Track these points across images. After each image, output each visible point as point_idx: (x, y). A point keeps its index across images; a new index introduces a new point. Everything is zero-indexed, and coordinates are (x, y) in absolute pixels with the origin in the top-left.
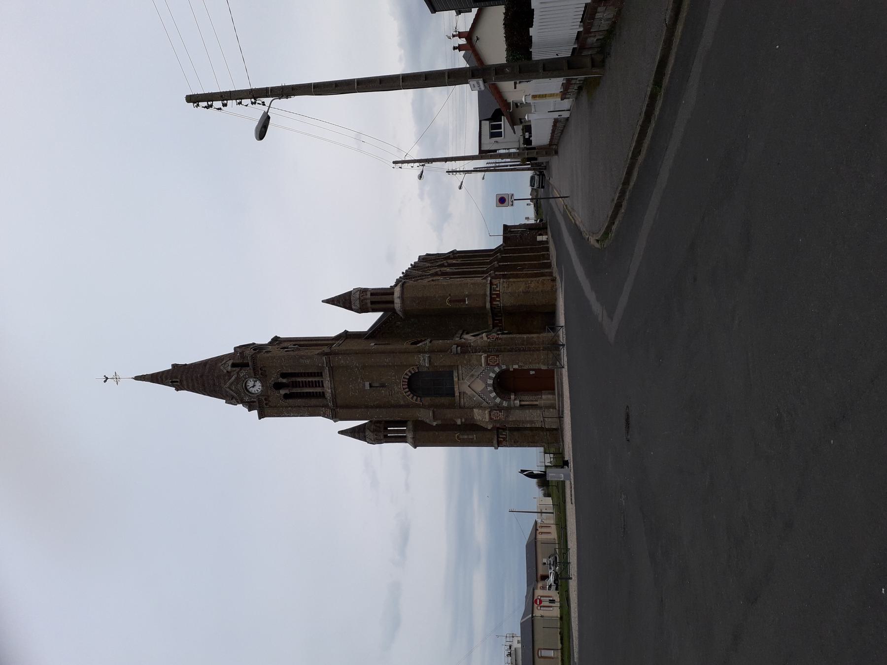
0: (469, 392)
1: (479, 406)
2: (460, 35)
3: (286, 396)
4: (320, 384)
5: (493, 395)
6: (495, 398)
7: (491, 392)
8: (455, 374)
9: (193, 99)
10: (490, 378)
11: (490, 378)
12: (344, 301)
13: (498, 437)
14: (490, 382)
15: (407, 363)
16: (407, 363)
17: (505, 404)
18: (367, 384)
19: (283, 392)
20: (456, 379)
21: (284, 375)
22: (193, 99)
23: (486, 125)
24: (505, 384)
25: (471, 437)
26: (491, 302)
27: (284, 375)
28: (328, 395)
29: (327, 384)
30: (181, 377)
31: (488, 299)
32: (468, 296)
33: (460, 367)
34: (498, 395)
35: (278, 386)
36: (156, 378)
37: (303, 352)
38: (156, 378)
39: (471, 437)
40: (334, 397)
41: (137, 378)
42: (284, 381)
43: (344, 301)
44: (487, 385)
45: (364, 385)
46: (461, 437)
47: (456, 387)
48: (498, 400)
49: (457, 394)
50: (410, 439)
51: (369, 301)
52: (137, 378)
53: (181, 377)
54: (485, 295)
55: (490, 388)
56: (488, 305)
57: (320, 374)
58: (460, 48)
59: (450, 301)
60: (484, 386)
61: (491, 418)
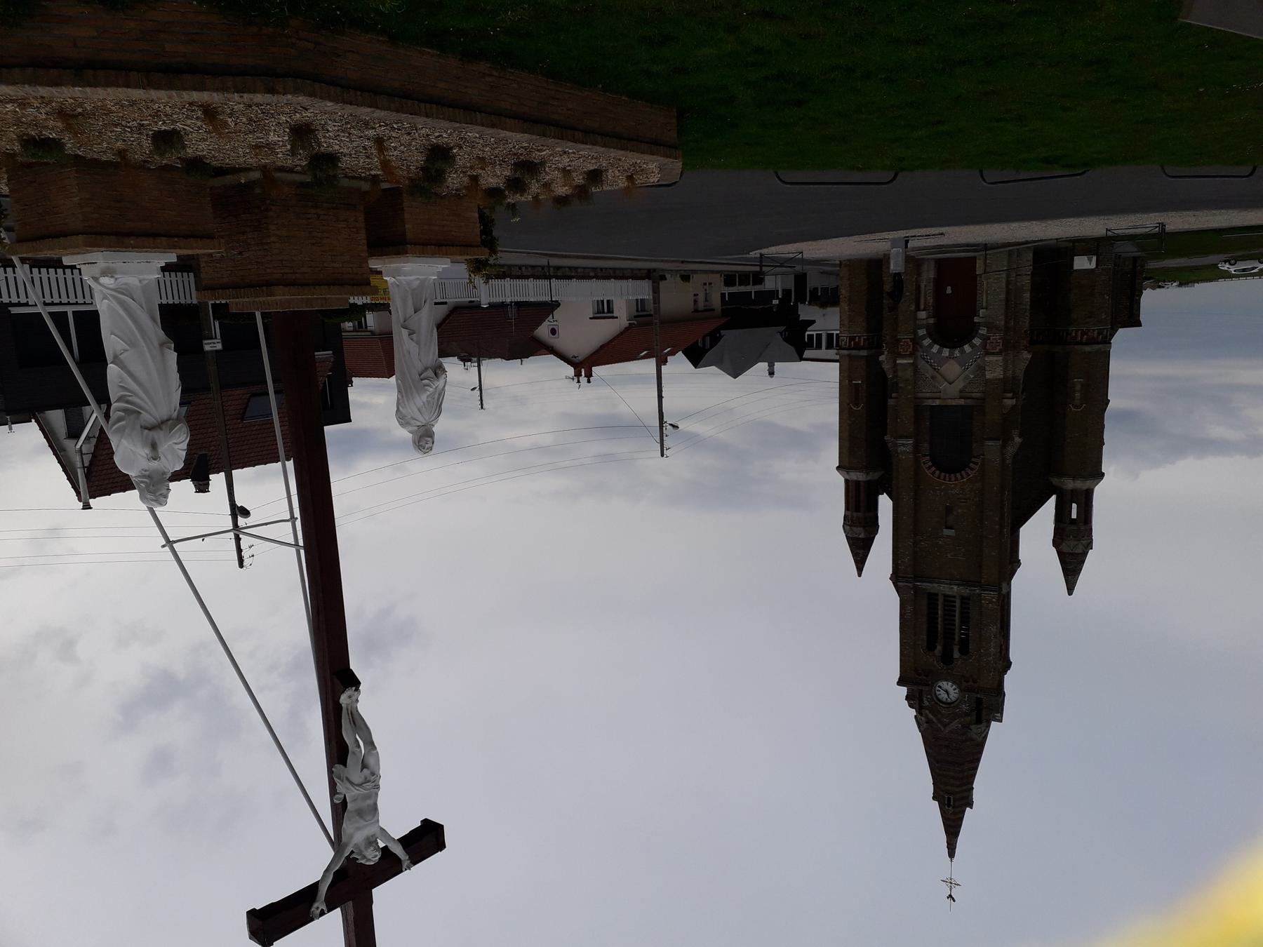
0: (959, 385)
1: (981, 369)
2: (578, 374)
3: (964, 650)
4: (948, 599)
5: (967, 348)
6: (973, 346)
7: (963, 352)
8: (929, 402)
10: (940, 352)
11: (940, 352)
12: (860, 549)
13: (1081, 343)
14: (946, 352)
15: (967, 480)
16: (967, 480)
17: (983, 331)
18: (946, 532)
19: (956, 655)
20: (938, 402)
21: (931, 647)
23: (807, 354)
24: (953, 329)
25: (1078, 387)
26: (863, 348)
27: (931, 647)
28: (965, 591)
29: (944, 589)
30: (953, 794)
31: (854, 352)
32: (850, 381)
33: (920, 395)
34: (969, 341)
35: (947, 658)
36: (952, 828)
37: (994, 629)
38: (952, 828)
39: (1078, 387)
40: (964, 582)
41: (952, 854)
42: (939, 648)
43: (860, 549)
44: (951, 357)
45: (948, 537)
46: (1077, 402)
47: (950, 402)
48: (977, 341)
49: (962, 402)
50: (1088, 484)
51: (855, 514)
52: (952, 854)
53: (953, 794)
54: (849, 356)
55: (957, 353)
56: (864, 353)
57: (932, 597)
58: (589, 375)
59: (857, 405)
60: (952, 361)
61: (999, 353)
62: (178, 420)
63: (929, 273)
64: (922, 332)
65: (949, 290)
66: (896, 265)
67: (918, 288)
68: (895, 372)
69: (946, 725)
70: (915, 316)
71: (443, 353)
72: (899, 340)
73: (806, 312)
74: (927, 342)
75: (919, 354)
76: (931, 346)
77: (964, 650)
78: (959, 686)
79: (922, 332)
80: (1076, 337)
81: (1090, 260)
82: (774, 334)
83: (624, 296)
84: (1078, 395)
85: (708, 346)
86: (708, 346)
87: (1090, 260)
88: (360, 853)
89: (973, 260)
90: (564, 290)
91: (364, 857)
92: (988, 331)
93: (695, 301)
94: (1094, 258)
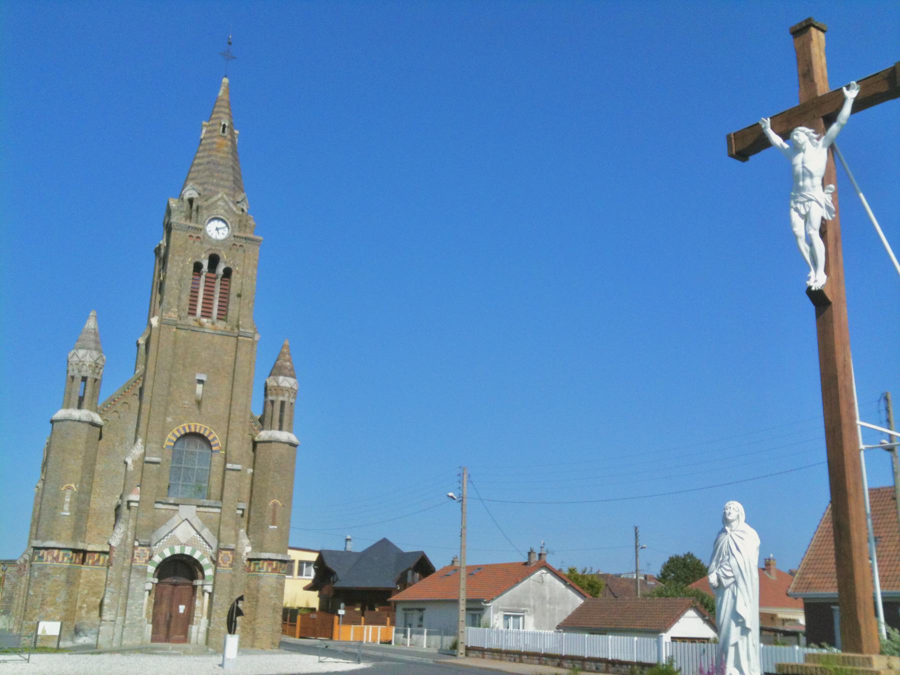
6: (161, 554)
7: (172, 549)
9: (636, 528)
10: (194, 551)
21: (228, 273)
22: (636, 528)
24: (180, 569)
25: (66, 507)
27: (228, 273)
35: (214, 260)
39: (66, 507)
44: (183, 545)
46: (69, 493)
59: (275, 505)
60: (183, 541)
62: (658, 661)
63: (198, 630)
64: (209, 572)
65: (182, 608)
66: (233, 641)
67: (209, 617)
68: (237, 535)
69: (222, 198)
70: (213, 589)
71: (893, 489)
72: (231, 565)
73: (313, 600)
74: (205, 562)
75: (214, 550)
76: (202, 557)
77: (198, 267)
78: (206, 234)
79: (85, 606)
80: (64, 555)
81: (44, 631)
82: (345, 579)
83: (498, 627)
84: (67, 500)
85: (410, 573)
86: (410, 573)
87: (44, 631)
88: (811, 139)
89: (153, 640)
90: (549, 640)
91: (807, 134)
92: (146, 568)
93: (421, 619)
94: (39, 632)
